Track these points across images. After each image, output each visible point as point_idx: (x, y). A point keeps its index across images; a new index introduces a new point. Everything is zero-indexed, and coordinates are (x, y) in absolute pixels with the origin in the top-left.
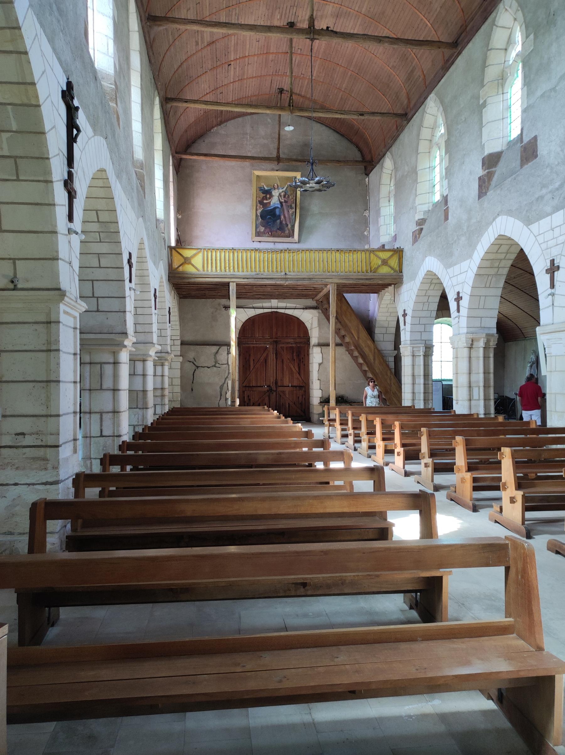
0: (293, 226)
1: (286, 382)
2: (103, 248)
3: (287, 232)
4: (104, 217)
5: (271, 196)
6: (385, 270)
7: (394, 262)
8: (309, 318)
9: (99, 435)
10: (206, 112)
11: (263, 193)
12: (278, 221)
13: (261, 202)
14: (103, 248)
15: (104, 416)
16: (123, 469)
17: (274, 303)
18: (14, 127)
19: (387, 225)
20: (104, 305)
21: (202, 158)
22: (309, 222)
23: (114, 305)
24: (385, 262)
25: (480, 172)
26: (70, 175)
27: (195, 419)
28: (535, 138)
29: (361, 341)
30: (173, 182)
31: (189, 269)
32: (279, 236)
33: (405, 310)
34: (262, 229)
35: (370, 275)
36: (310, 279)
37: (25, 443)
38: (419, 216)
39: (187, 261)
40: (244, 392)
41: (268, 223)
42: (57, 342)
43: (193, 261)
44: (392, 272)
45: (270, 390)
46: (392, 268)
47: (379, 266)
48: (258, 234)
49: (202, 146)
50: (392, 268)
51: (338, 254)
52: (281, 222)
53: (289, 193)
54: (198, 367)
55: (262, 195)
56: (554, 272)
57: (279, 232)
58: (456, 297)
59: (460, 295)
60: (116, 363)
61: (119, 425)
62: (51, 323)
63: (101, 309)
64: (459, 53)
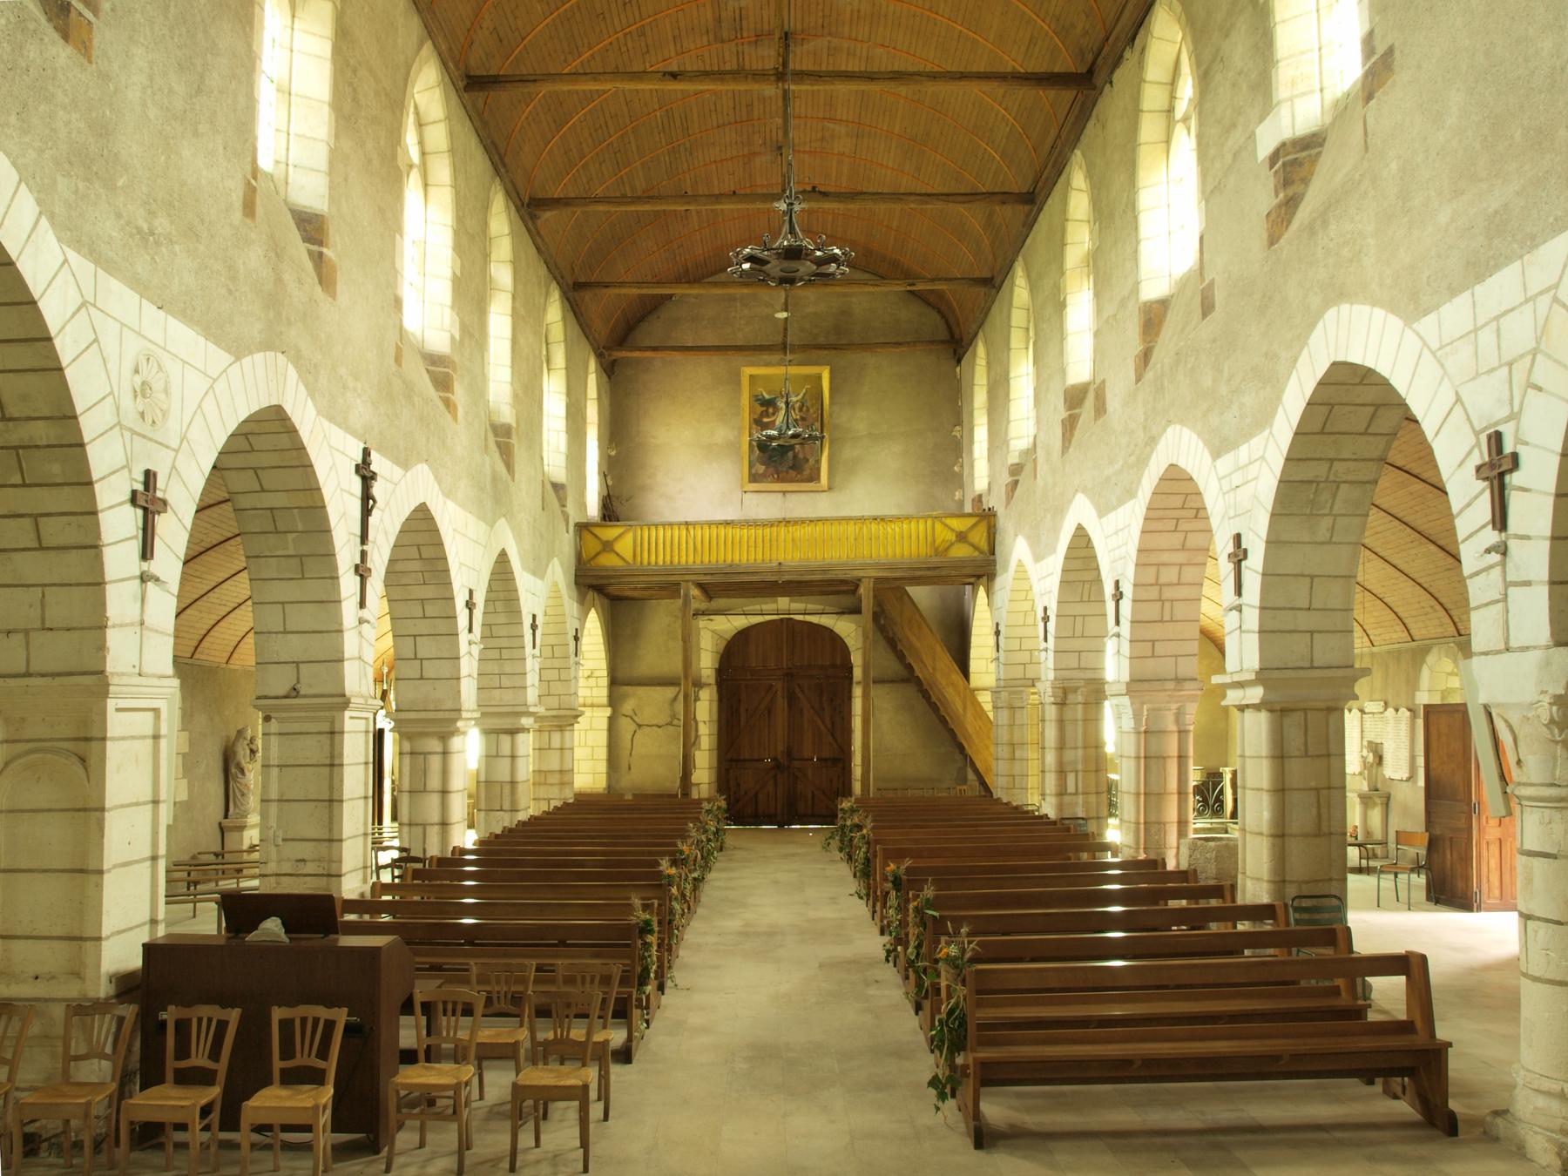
0: (818, 462)
3: (807, 472)
4: (427, 552)
6: (961, 552)
7: (979, 537)
8: (847, 629)
10: (641, 296)
11: (762, 405)
12: (790, 454)
14: (428, 592)
15: (429, 829)
16: (1290, 953)
17: (783, 603)
18: (300, 528)
19: (1013, 407)
21: (648, 354)
22: (848, 453)
23: (444, 669)
24: (962, 537)
25: (1063, 413)
26: (363, 554)
27: (519, 844)
29: (938, 675)
30: (599, 398)
31: (608, 560)
33: (1238, 539)
34: (761, 469)
38: (1013, 459)
39: (608, 546)
40: (727, 770)
41: (771, 457)
42: (341, 755)
43: (618, 547)
44: (976, 554)
45: (777, 765)
48: (754, 478)
49: (654, 330)
52: (795, 457)
54: (640, 726)
55: (760, 409)
57: (793, 473)
58: (1481, 456)
59: (1508, 448)
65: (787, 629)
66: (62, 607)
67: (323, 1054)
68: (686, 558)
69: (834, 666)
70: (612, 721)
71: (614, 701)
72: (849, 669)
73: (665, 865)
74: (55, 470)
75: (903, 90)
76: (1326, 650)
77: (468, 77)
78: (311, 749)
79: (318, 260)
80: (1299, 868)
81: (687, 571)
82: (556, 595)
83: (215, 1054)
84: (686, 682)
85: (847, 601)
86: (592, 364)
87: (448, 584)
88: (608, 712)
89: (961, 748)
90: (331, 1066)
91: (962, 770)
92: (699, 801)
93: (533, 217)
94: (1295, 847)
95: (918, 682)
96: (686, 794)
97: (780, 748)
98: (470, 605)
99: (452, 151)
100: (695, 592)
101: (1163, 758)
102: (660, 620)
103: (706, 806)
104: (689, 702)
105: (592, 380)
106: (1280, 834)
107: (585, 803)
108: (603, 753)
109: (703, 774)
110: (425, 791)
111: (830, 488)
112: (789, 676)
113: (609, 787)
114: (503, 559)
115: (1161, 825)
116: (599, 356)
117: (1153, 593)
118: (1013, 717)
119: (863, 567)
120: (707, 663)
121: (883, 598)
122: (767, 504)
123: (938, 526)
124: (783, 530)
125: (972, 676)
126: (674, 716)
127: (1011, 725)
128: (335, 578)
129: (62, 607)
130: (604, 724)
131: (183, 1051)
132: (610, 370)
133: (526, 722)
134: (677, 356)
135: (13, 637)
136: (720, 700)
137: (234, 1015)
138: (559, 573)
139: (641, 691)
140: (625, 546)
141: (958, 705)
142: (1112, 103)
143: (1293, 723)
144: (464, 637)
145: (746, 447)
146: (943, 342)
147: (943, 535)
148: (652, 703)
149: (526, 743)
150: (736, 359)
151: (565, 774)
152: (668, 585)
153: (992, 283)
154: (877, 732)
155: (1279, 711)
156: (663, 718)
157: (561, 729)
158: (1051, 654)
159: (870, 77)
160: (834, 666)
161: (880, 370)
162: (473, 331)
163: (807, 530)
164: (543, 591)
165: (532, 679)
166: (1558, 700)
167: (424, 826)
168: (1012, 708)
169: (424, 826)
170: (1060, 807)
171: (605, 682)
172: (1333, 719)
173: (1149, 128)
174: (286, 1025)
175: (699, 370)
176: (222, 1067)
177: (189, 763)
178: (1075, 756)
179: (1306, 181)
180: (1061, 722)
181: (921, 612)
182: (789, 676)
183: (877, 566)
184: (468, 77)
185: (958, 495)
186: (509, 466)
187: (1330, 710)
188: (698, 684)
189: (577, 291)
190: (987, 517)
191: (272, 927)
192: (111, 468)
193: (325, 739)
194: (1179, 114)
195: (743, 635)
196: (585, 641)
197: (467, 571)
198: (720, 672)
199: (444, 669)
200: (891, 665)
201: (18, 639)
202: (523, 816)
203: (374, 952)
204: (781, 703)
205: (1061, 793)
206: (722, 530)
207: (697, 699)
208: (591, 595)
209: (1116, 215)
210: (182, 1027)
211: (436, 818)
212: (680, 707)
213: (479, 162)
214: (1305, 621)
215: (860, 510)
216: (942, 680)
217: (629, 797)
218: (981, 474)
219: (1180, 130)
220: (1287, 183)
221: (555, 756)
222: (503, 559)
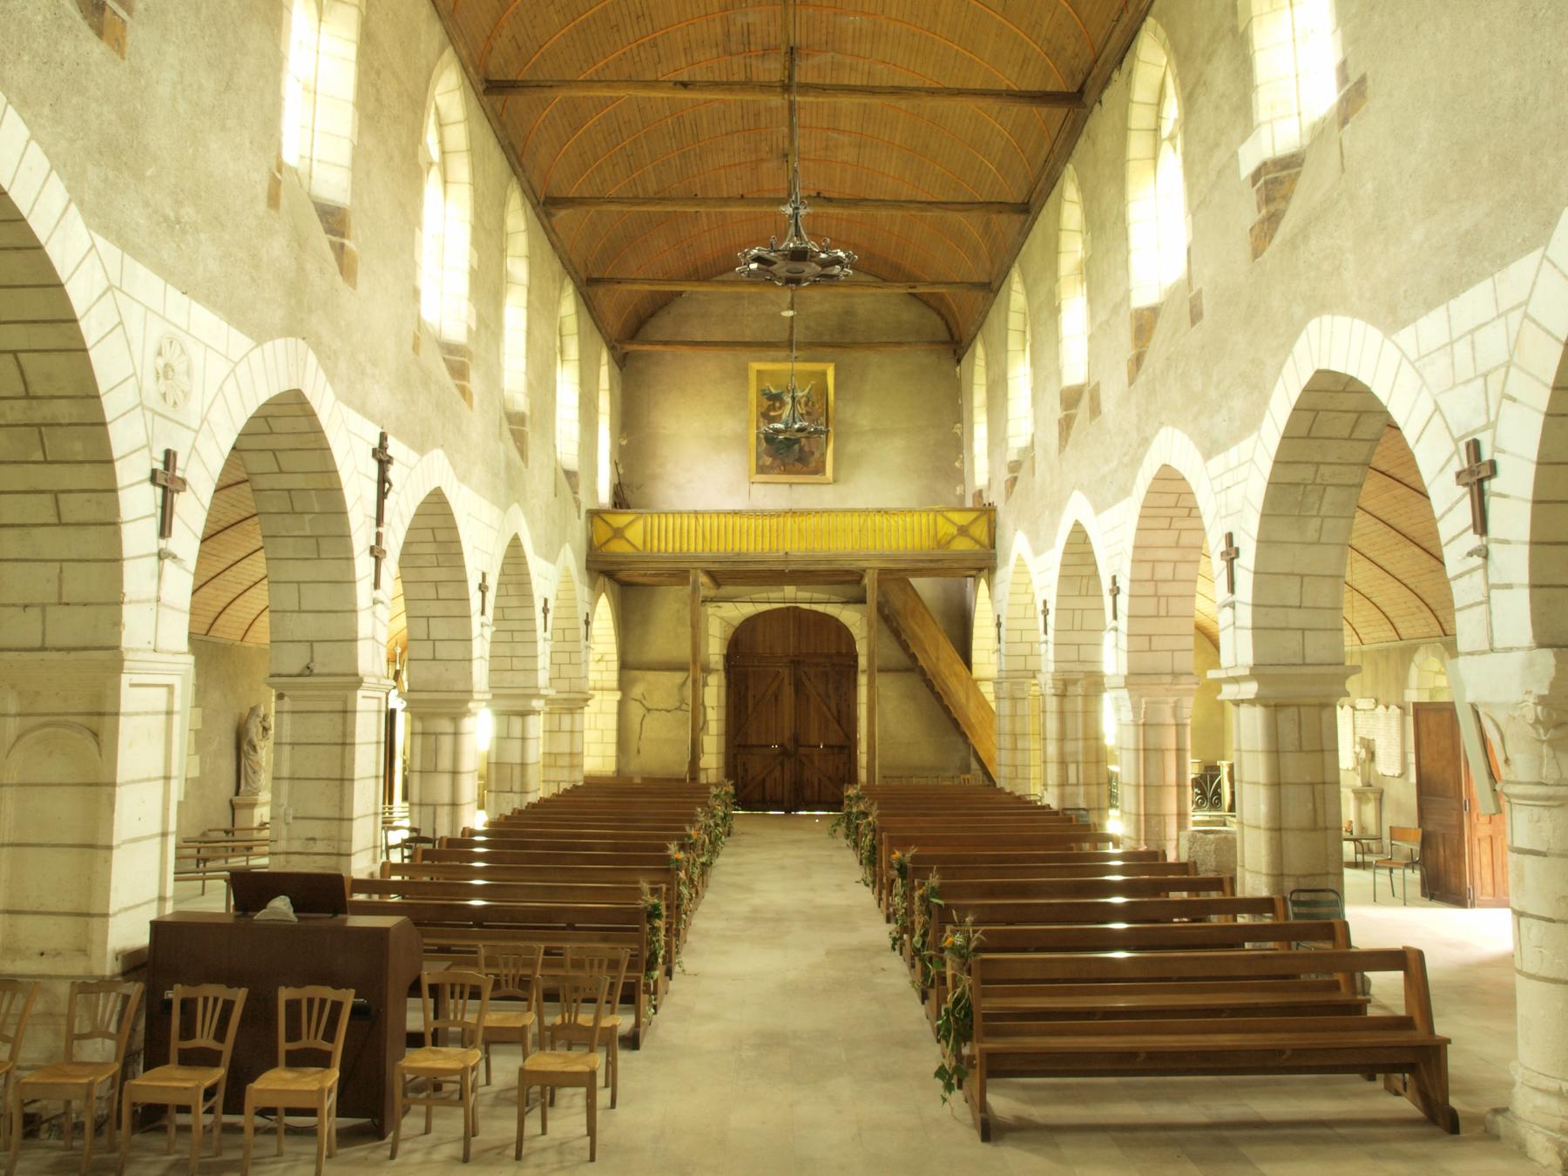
0: (823, 455)
1: (814, 737)
2: (442, 574)
4: (442, 535)
6: (962, 545)
7: (980, 531)
8: (851, 618)
9: (1486, 647)
10: (652, 292)
14: (442, 574)
17: (790, 591)
20: (443, 650)
21: (659, 348)
22: (852, 447)
23: (455, 650)
24: (963, 531)
25: (1059, 413)
26: (379, 536)
28: (1098, 384)
31: (618, 547)
32: (798, 473)
33: (1230, 538)
34: (768, 461)
35: (938, 553)
36: (830, 561)
37: (316, 850)
38: (1012, 456)
39: (618, 533)
41: (778, 450)
42: (353, 734)
43: (629, 534)
44: (977, 547)
45: (784, 752)
46: (977, 542)
47: (954, 537)
48: (761, 469)
49: (664, 325)
50: (977, 542)
51: (878, 518)
52: (801, 449)
53: (814, 398)
54: (649, 710)
55: (767, 403)
56: (1481, 481)
57: (799, 466)
59: (1486, 455)
61: (1159, 801)
62: (347, 713)
63: (438, 656)
64: (1035, 219)
65: (795, 617)
66: (79, 582)
67: (330, 1036)
69: (839, 654)
70: (622, 706)
71: (624, 685)
73: (673, 850)
74: (77, 448)
75: (903, 104)
76: (1316, 648)
78: (323, 728)
79: (340, 250)
80: (1297, 862)
81: (697, 559)
82: (567, 579)
83: (220, 1035)
84: (694, 667)
85: (852, 591)
88: (618, 696)
89: (964, 735)
92: (707, 786)
93: (549, 215)
96: (694, 778)
97: (787, 734)
98: (483, 588)
100: (703, 579)
102: (669, 607)
103: (714, 791)
104: (697, 687)
106: (1277, 829)
107: (594, 785)
108: (612, 736)
109: (712, 759)
110: (436, 771)
111: (835, 481)
112: (796, 663)
113: (618, 770)
114: (515, 543)
115: (1161, 816)
117: (1149, 589)
118: (1014, 707)
119: (867, 558)
120: (715, 650)
122: (775, 494)
123: (940, 520)
124: (789, 520)
125: (974, 667)
126: (682, 701)
127: (1013, 716)
128: (350, 559)
129: (79, 582)
130: (614, 708)
131: (188, 1031)
132: (622, 361)
133: (537, 704)
137: (240, 995)
138: (571, 559)
139: (650, 675)
140: (635, 533)
142: (1101, 121)
143: (1287, 718)
144: (476, 619)
145: (753, 440)
146: (943, 343)
147: (946, 529)
148: (660, 687)
149: (537, 726)
150: (743, 354)
151: (575, 757)
152: (677, 573)
153: (991, 288)
154: (882, 719)
155: (1274, 706)
156: (672, 703)
157: (571, 711)
158: (1051, 647)
159: (872, 91)
160: (839, 654)
161: (882, 369)
163: (812, 521)
164: (555, 575)
165: (543, 661)
166: (1542, 700)
168: (1014, 699)
169: (435, 806)
170: (1062, 797)
171: (615, 666)
172: (1325, 715)
173: (1137, 146)
174: (293, 1006)
175: (709, 365)
176: (227, 1048)
177: (201, 740)
179: (1286, 198)
180: (1062, 714)
181: (923, 609)
182: (796, 663)
183: (882, 557)
185: (959, 490)
186: (523, 453)
188: (707, 670)
189: (590, 286)
190: (987, 512)
191: (281, 906)
192: (132, 448)
193: (338, 718)
195: (750, 623)
197: (481, 555)
199: (455, 650)
200: (891, 652)
201: (34, 613)
202: (533, 798)
205: (1063, 783)
206: (730, 520)
207: (705, 684)
208: (602, 580)
210: (188, 1006)
212: (688, 692)
213: (497, 161)
214: (1296, 618)
215: (865, 503)
217: (638, 780)
218: (981, 470)
220: (1268, 200)
222: (515, 543)
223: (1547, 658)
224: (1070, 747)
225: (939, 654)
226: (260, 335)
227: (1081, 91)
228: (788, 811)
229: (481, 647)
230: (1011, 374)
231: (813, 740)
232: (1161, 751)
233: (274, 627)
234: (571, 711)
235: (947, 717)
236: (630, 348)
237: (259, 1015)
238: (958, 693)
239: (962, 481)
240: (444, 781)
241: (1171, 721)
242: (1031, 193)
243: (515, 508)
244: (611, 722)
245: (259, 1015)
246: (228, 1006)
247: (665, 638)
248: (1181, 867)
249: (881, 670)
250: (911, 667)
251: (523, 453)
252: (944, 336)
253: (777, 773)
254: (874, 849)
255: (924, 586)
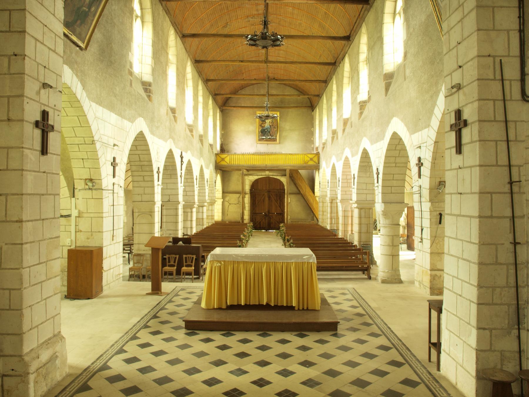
1: (273, 211)
5: (265, 123)
6: (311, 163)
7: (316, 159)
8: (284, 180)
13: (261, 126)
17: (267, 173)
19: (322, 133)
22: (284, 134)
23: (191, 193)
24: (311, 159)
31: (223, 163)
35: (305, 165)
38: (324, 141)
39: (223, 159)
43: (226, 160)
45: (266, 215)
46: (315, 162)
48: (260, 140)
50: (315, 162)
55: (261, 122)
60: (192, 212)
61: (347, 228)
65: (268, 179)
66: (147, 190)
67: (192, 262)
68: (242, 163)
69: (280, 189)
70: (223, 203)
71: (223, 197)
72: (284, 190)
73: (242, 236)
74: (147, 169)
75: (293, 65)
76: (369, 197)
77: (196, 61)
78: (172, 212)
79: (174, 117)
80: (363, 239)
81: (243, 166)
82: (211, 172)
83: (175, 262)
84: (242, 193)
85: (283, 173)
86: (218, 111)
87: (193, 175)
88: (222, 200)
89: (313, 212)
90: (193, 264)
91: (313, 217)
92: (246, 224)
93: (207, 83)
94: (363, 235)
95: (302, 195)
96: (243, 222)
97: (266, 210)
99: (193, 78)
100: (245, 170)
101: (348, 217)
102: (235, 177)
103: (248, 225)
104: (243, 198)
105: (218, 114)
106: (360, 233)
107: (217, 223)
108: (221, 211)
109: (247, 217)
111: (279, 143)
112: (269, 191)
113: (222, 220)
114: (202, 167)
115: (347, 231)
116: (220, 108)
117: (346, 181)
118: (323, 205)
119: (287, 166)
120: (247, 188)
121: (293, 174)
122: (263, 147)
123: (306, 156)
124: (267, 156)
125: (315, 193)
126: (239, 202)
127: (323, 207)
128: (177, 179)
129: (147, 190)
130: (221, 204)
131: (169, 262)
132: (222, 111)
133: (206, 204)
134: (240, 108)
135: (43, 171)
136: (251, 198)
137: (178, 256)
138: (212, 167)
139: (231, 195)
140: (227, 160)
141: (312, 201)
142: (339, 70)
143: (363, 211)
144: (196, 186)
145: (258, 132)
146: (308, 107)
147: (307, 159)
148: (233, 198)
149: (205, 209)
150: (255, 109)
151: (213, 216)
152: (238, 169)
153: (319, 96)
154: (292, 207)
155: (360, 209)
156: (236, 202)
157: (212, 205)
159: (286, 63)
160: (280, 189)
161: (292, 113)
162: (196, 117)
163: (273, 157)
164: (209, 172)
165: (207, 194)
166: (382, 211)
167: (187, 228)
168: (323, 202)
169: (187, 228)
170: (331, 227)
171: (221, 192)
172: (371, 210)
174: (186, 258)
175: (246, 112)
176: (176, 264)
177: (127, 213)
178: (334, 215)
179: (364, 109)
180: (331, 207)
181: (302, 179)
182: (269, 191)
183: (290, 166)
184: (196, 61)
185: (312, 146)
186: (202, 144)
187: (370, 209)
188: (246, 194)
189: (215, 95)
190: (318, 154)
191: (181, 243)
193: (175, 210)
194: (397, 11)
195: (257, 181)
196: (217, 182)
197: (196, 173)
198: (251, 190)
199: (191, 193)
200: (294, 189)
201: (140, 196)
202: (205, 226)
203: (199, 247)
204: (267, 199)
205: (331, 224)
206: (252, 156)
207: (245, 197)
208: (218, 170)
209: (377, 41)
210: (169, 258)
211: (189, 226)
212: (241, 199)
213: (196, 75)
214: (365, 192)
215: (287, 150)
216: (307, 194)
217: (227, 222)
218: (317, 143)
219: (397, 17)
220: (361, 109)
221: (210, 212)
222: (202, 167)
223: (383, 204)
224: (333, 215)
225: (306, 190)
226: (166, 141)
227: (335, 62)
228: (266, 230)
229: (196, 193)
230: (323, 120)
231: (273, 211)
232: (348, 217)
233: (133, 184)
234: (212, 205)
235: (309, 208)
236: (224, 108)
237: (181, 259)
238: (311, 200)
239: (313, 143)
240: (189, 222)
241: (350, 210)
242: (327, 78)
243: (201, 158)
244: (220, 207)
245: (181, 259)
246: (176, 258)
247: (235, 185)
248: (341, 238)
249: (290, 194)
250: (299, 193)
251: (202, 144)
252: (310, 105)
253: (264, 220)
254: (284, 237)
255: (302, 172)
